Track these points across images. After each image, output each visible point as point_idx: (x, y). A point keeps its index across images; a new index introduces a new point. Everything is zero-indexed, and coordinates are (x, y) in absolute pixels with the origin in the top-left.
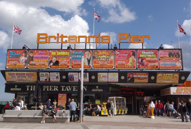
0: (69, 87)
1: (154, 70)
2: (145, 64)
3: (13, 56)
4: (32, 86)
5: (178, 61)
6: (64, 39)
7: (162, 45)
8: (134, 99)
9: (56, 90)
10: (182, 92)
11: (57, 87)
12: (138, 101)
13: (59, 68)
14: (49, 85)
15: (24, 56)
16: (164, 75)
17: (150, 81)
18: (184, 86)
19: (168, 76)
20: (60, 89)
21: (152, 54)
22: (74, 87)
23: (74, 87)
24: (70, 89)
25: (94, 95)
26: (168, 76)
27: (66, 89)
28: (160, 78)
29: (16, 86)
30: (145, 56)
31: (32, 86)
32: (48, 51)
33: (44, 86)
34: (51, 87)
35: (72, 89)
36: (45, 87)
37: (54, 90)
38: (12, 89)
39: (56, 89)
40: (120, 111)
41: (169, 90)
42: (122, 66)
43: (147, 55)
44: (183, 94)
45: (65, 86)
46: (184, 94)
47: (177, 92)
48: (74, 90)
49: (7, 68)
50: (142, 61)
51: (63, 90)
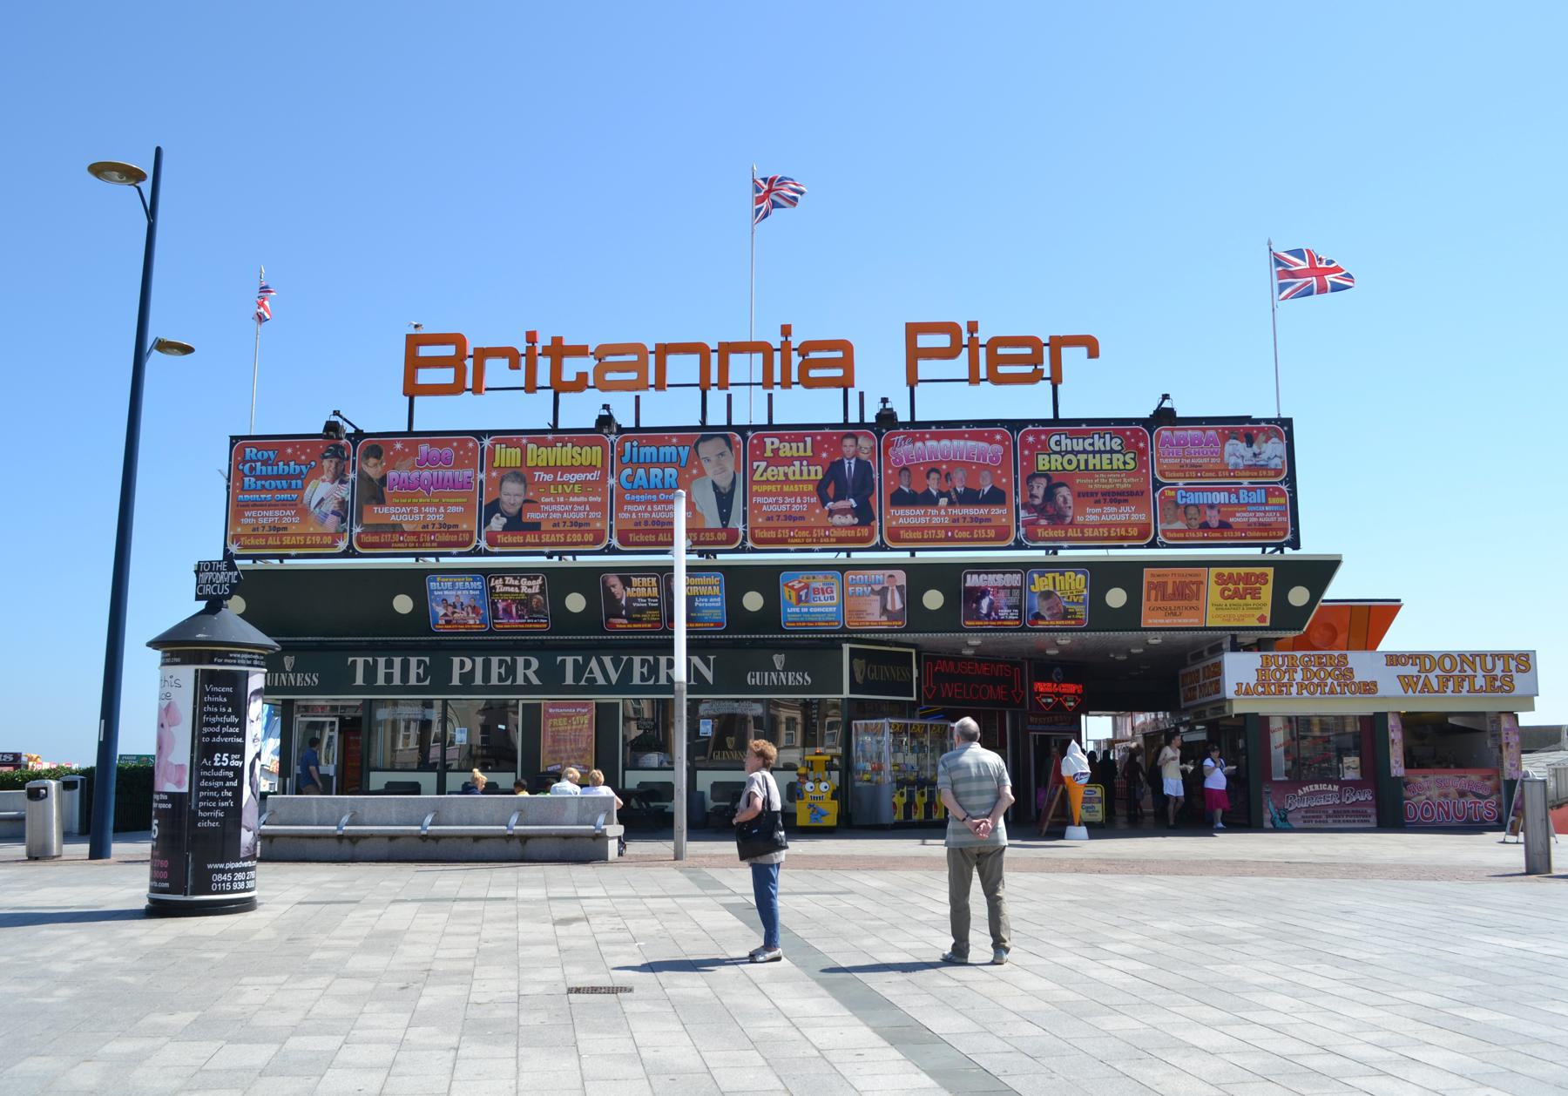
0: (607, 660)
3: (267, 477)
4: (382, 661)
10: (1292, 679)
11: (535, 663)
21: (1112, 451)
22: (637, 660)
23: (637, 660)
27: (591, 672)
30: (1070, 462)
33: (456, 660)
34: (419, 663)
36: (462, 665)
41: (1218, 670)
43: (1082, 457)
50: (1050, 494)
51: (569, 680)
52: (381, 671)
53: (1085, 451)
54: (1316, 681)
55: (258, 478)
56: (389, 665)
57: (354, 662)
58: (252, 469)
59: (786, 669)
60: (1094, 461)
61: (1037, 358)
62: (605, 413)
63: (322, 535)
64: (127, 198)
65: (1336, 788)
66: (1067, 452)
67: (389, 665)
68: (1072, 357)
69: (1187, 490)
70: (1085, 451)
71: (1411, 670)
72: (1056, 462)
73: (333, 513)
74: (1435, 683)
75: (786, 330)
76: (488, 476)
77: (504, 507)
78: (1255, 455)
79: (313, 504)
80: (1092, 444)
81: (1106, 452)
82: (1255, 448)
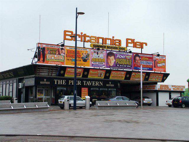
0: (89, 82)
4: (59, 80)
6: (87, 39)
7: (146, 45)
11: (80, 82)
17: (126, 78)
20: (82, 83)
22: (93, 82)
23: (93, 82)
24: (90, 84)
25: (20, 84)
29: (110, 83)
33: (70, 81)
34: (64, 81)
35: (92, 84)
36: (71, 81)
39: (79, 83)
47: (160, 88)
48: (93, 85)
51: (85, 85)
52: (59, 82)
56: (60, 81)
61: (141, 45)
67: (60, 81)
68: (144, 45)
71: (174, 87)
75: (113, 37)
78: (98, 57)
82: (98, 55)
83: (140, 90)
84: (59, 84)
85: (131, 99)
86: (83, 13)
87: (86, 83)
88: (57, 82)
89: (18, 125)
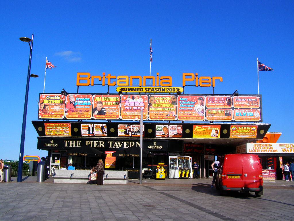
0: (119, 142)
1: (129, 120)
2: (48, 112)
3: (185, 104)
4: (71, 142)
5: (256, 111)
7: (236, 90)
8: (203, 159)
9: (102, 146)
10: (260, 149)
11: (104, 143)
12: (207, 161)
13: (106, 118)
14: (93, 140)
15: (199, 104)
16: (239, 128)
17: (222, 135)
18: (262, 142)
19: (243, 129)
20: (107, 145)
21: (58, 99)
22: (125, 143)
23: (125, 143)
24: (120, 146)
26: (243, 129)
27: (115, 145)
28: (234, 132)
30: (50, 101)
31: (71, 142)
32: (91, 96)
34: (79, 142)
35: (123, 145)
36: (88, 143)
37: (99, 146)
38: (46, 145)
39: (102, 145)
40: (184, 173)
41: (245, 147)
42: (186, 117)
43: (52, 100)
44: (261, 152)
45: (69, 141)
46: (263, 152)
47: (254, 149)
48: (125, 147)
49: (40, 117)
50: (45, 107)
51: (111, 147)
53: (53, 99)
54: (265, 149)
55: (183, 104)
56: (73, 142)
57: (65, 142)
58: (182, 102)
59: (156, 145)
60: (54, 101)
62: (63, 90)
63: (199, 117)
64: (26, 43)
65: (269, 171)
66: (49, 99)
67: (73, 142)
69: (219, 110)
70: (53, 99)
72: (47, 101)
73: (201, 112)
74: (289, 150)
76: (94, 103)
77: (98, 109)
79: (197, 110)
80: (54, 98)
81: (57, 99)
83: (230, 153)
84: (71, 146)
85: (193, 175)
86: (36, 76)
87: (113, 145)
88: (69, 144)
89: (119, 215)
